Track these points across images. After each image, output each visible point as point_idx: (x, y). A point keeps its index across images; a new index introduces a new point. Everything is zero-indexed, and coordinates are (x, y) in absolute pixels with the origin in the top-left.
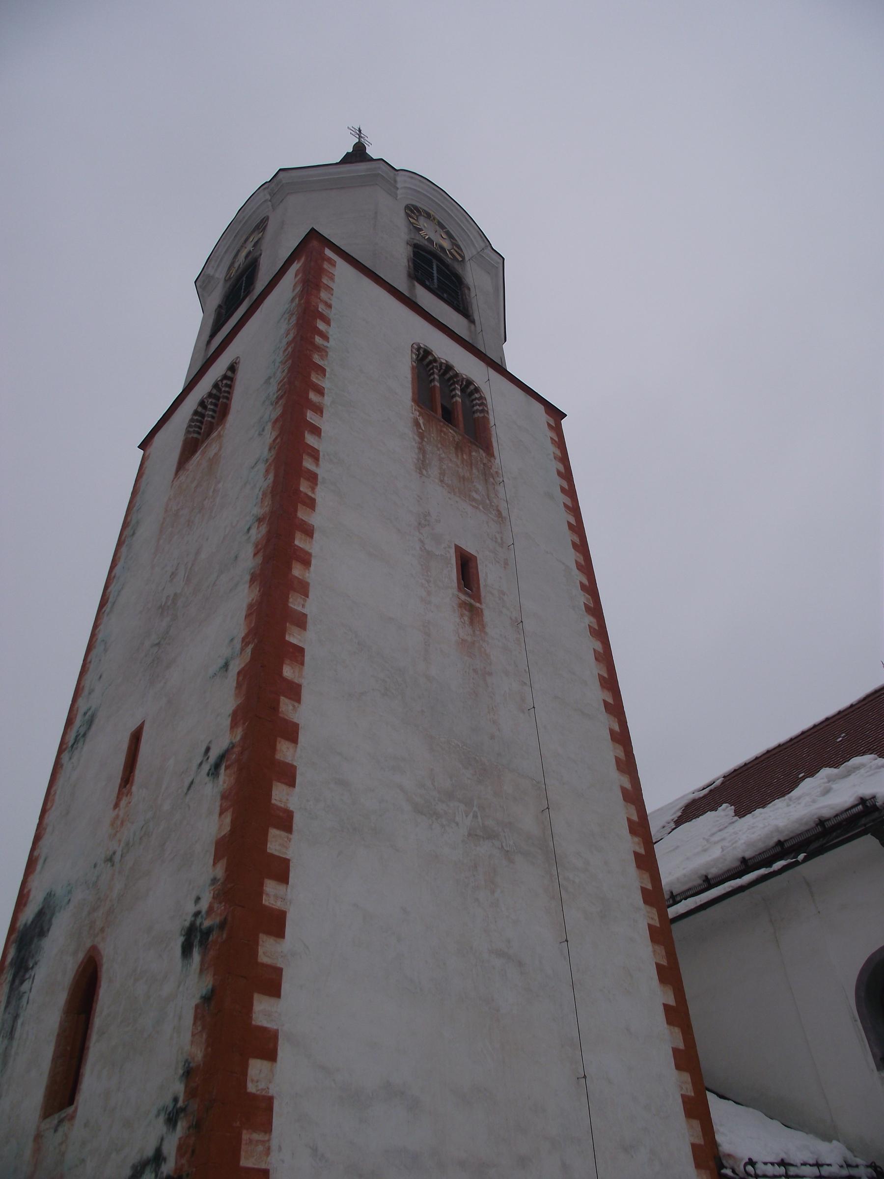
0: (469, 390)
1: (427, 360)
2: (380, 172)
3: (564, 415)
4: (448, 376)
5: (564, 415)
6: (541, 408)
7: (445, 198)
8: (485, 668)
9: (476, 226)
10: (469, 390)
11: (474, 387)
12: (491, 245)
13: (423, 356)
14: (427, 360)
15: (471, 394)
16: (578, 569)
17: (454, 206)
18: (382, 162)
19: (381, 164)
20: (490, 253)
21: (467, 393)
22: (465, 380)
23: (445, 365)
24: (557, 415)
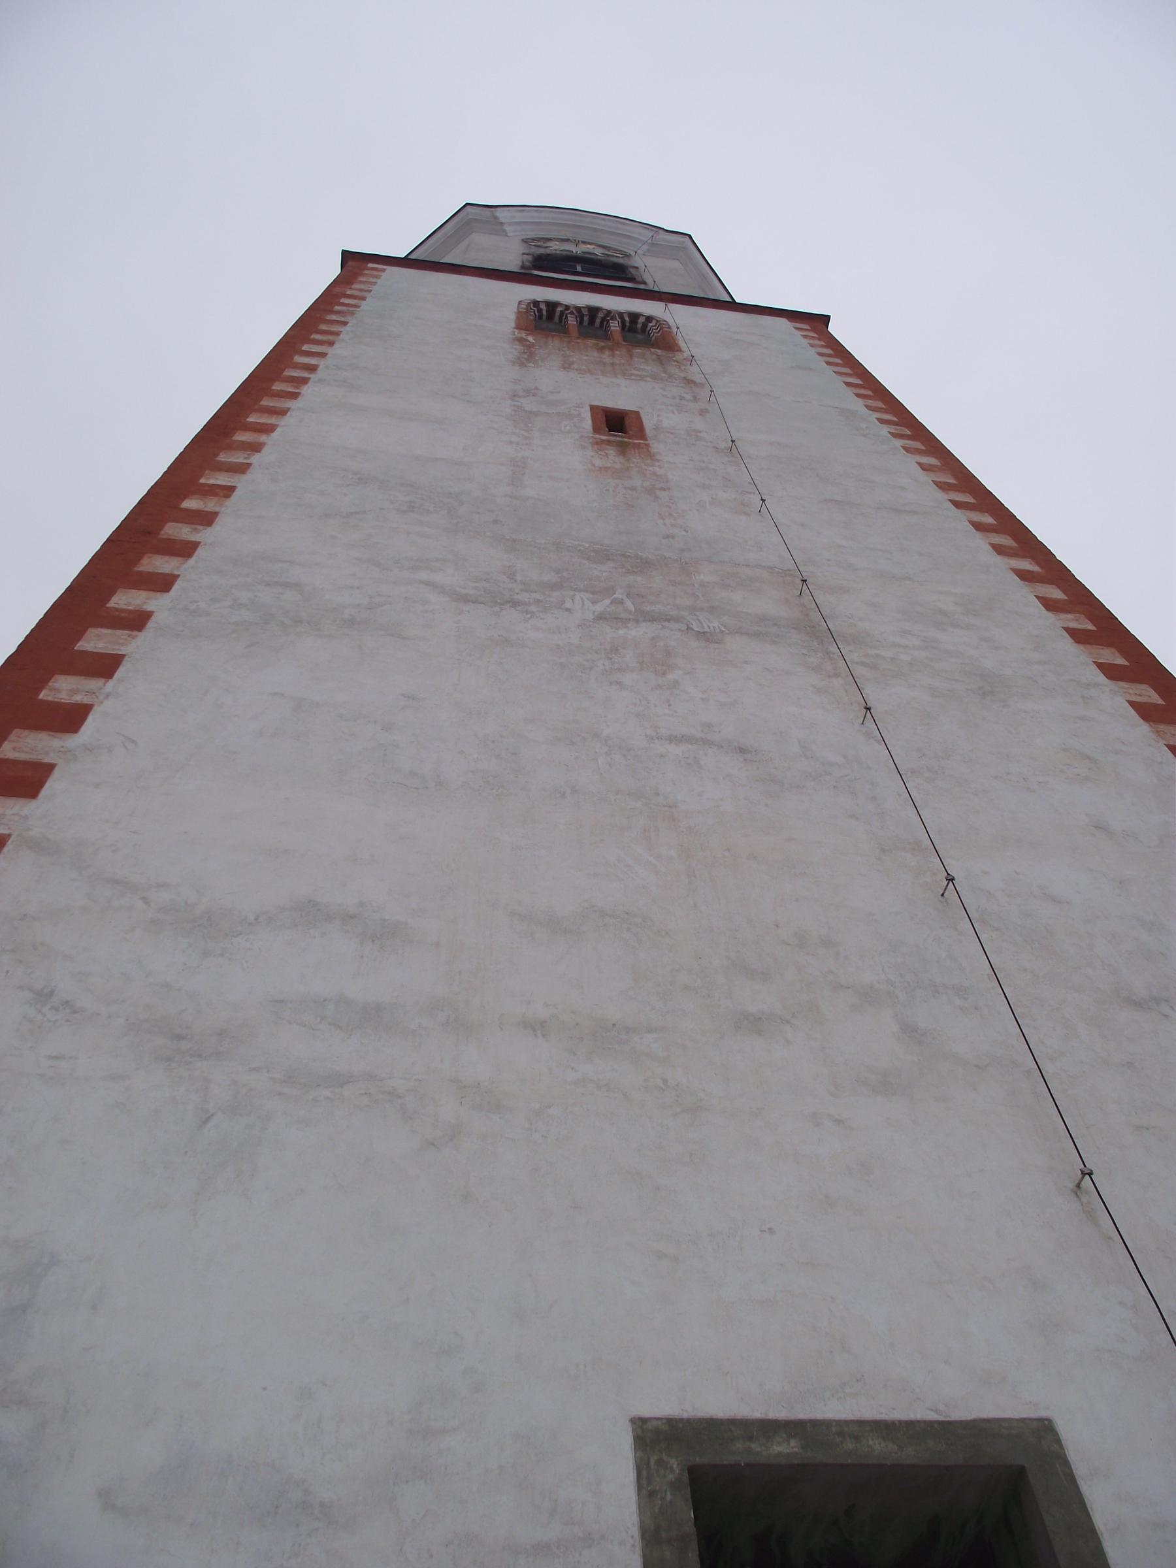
0: (639, 326)
1: (558, 314)
2: (471, 217)
3: (825, 319)
4: (598, 321)
5: (825, 319)
6: (783, 322)
7: (581, 216)
8: (594, 465)
9: (704, 262)
10: (639, 326)
11: (644, 318)
12: (663, 229)
13: (548, 311)
14: (558, 314)
15: (645, 326)
16: (868, 410)
17: (599, 218)
18: (468, 207)
19: (468, 208)
20: (665, 237)
21: (639, 331)
22: (625, 315)
23: (587, 309)
24: (819, 322)
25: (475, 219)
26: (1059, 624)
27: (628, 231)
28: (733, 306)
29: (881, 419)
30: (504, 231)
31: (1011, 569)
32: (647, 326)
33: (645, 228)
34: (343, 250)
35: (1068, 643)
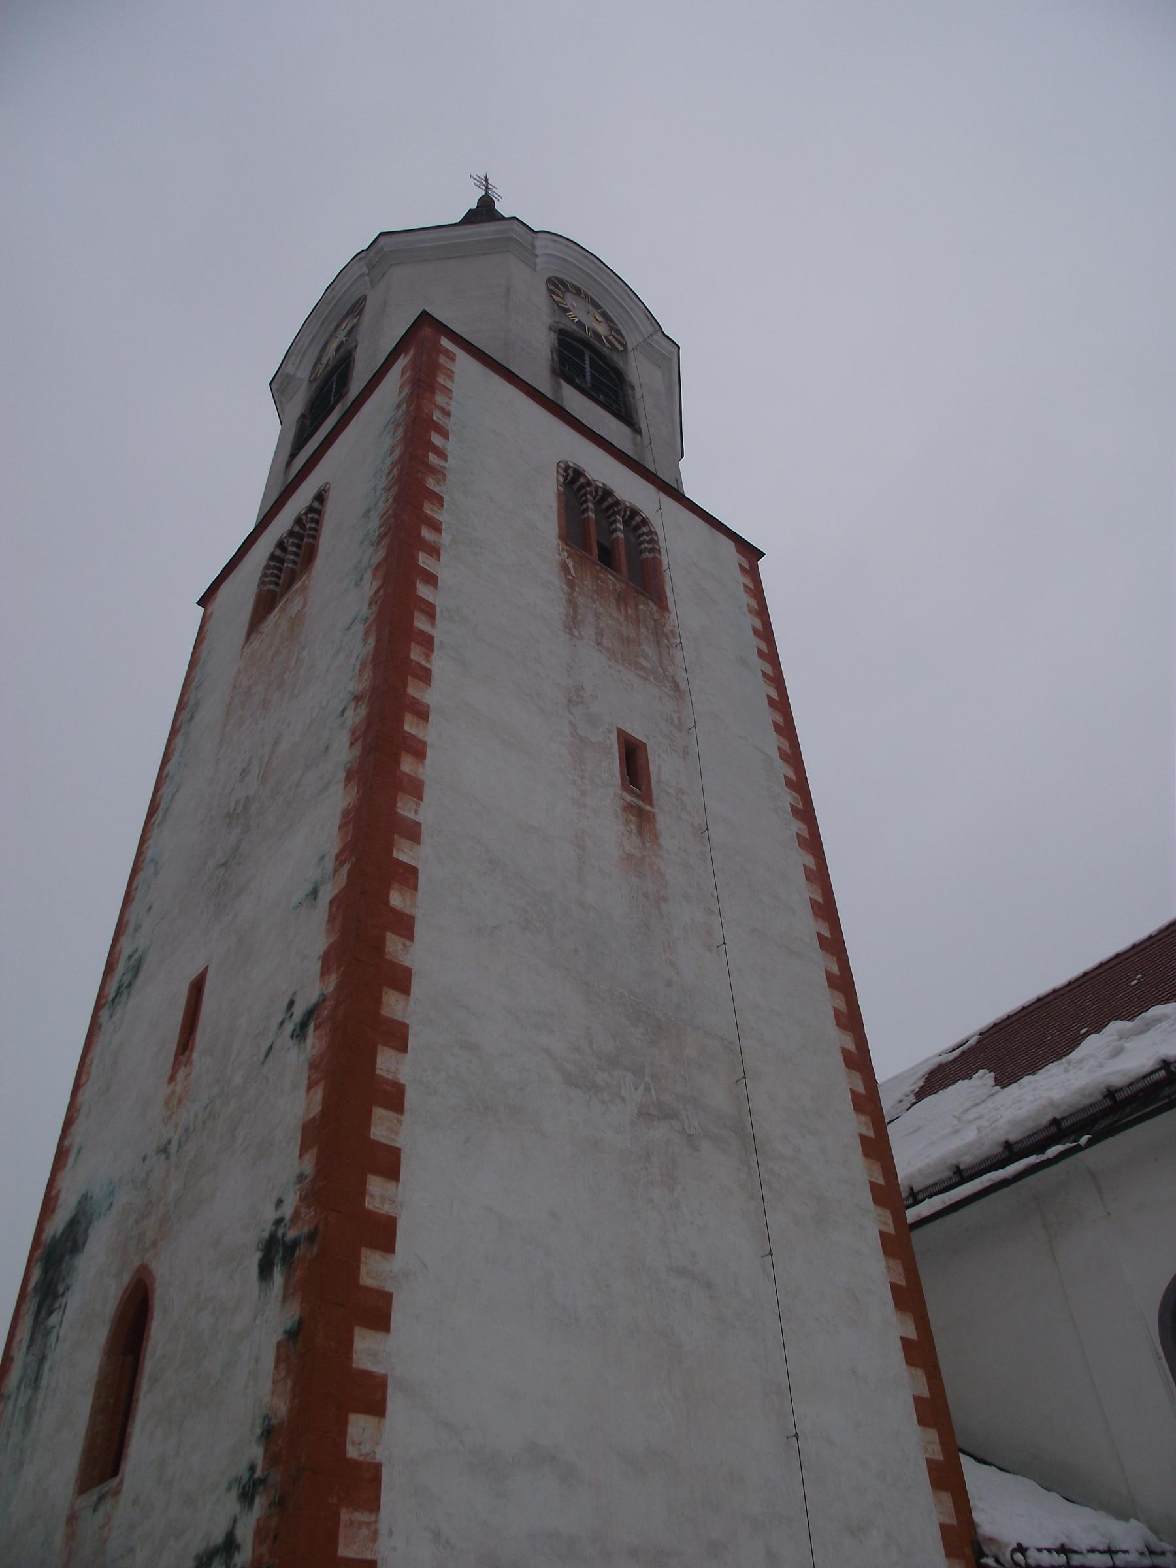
1: (579, 484)
2: (514, 235)
4: (605, 504)
6: (730, 545)
7: (600, 268)
10: (634, 523)
12: (661, 329)
14: (579, 484)
15: (638, 527)
24: (752, 554)
25: (516, 240)
26: (889, 1279)
27: (631, 309)
28: (676, 494)
29: (765, 673)
30: (535, 264)
31: (842, 1047)
32: (640, 528)
33: (646, 315)
34: (765, 554)
35: (742, 588)
